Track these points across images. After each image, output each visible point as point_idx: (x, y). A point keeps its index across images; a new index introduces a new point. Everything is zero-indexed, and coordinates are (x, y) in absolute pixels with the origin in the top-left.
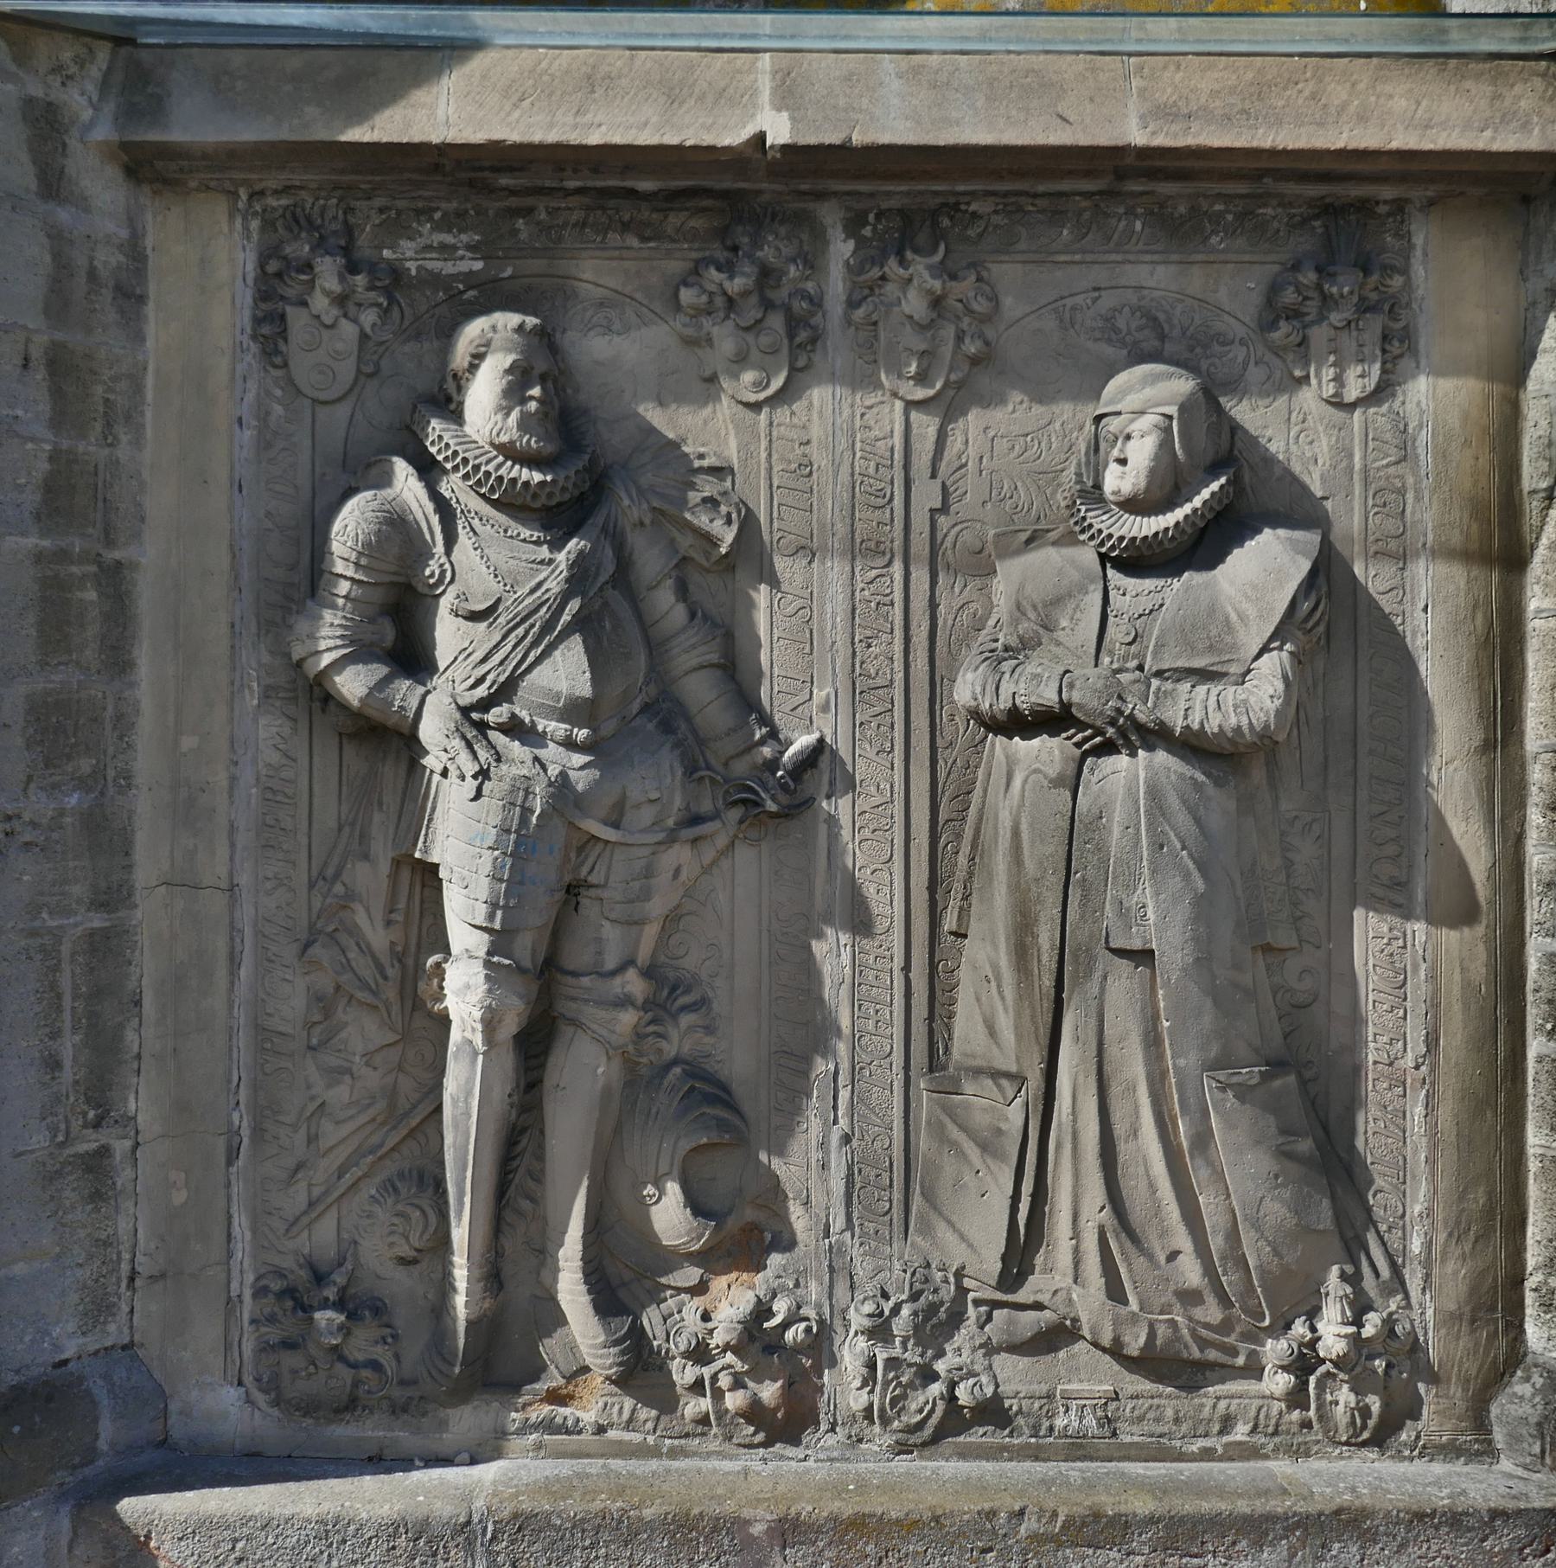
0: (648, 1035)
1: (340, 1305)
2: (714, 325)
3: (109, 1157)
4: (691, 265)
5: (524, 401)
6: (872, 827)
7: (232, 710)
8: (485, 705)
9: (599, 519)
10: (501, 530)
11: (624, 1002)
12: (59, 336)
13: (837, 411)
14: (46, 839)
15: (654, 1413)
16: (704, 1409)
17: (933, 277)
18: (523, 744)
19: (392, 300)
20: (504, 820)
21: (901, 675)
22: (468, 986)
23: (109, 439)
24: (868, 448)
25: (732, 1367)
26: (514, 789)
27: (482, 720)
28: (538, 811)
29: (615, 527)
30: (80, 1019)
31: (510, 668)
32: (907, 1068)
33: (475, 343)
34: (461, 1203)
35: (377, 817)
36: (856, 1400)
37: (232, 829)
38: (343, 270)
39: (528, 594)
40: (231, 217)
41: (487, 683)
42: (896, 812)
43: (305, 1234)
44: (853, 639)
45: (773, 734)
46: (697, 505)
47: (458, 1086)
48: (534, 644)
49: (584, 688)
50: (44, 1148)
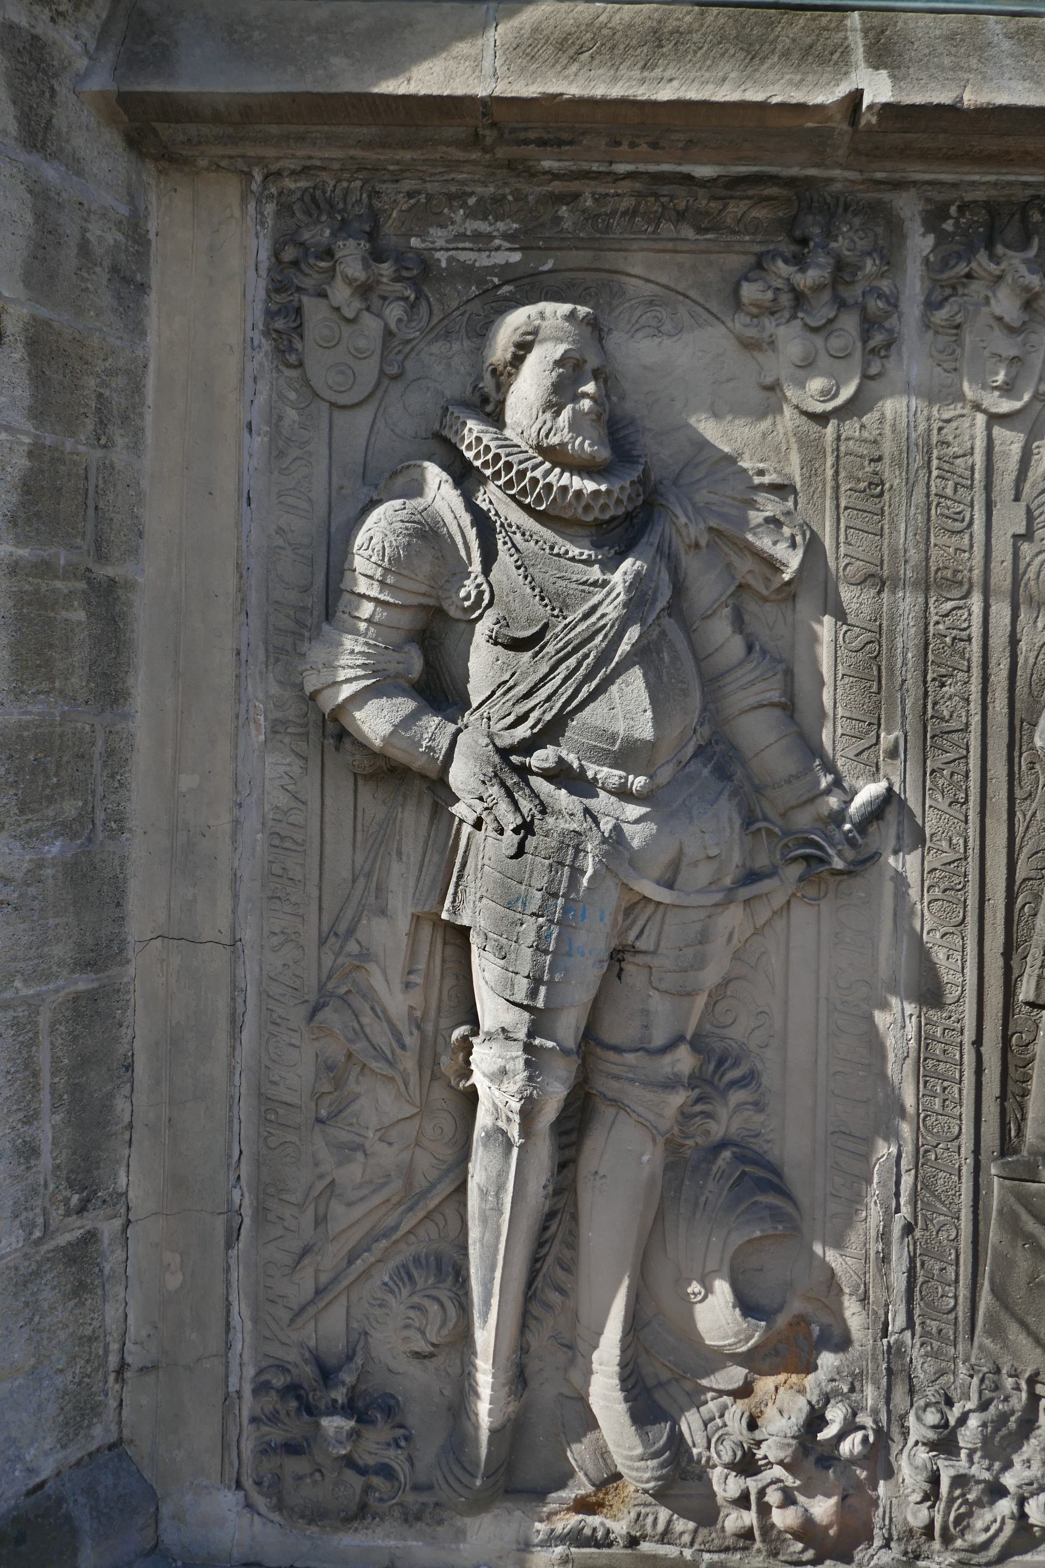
0: (695, 1115)
1: (348, 1409)
2: (778, 325)
3: (95, 1242)
4: (752, 259)
5: (576, 398)
6: (942, 887)
7: (236, 747)
8: (528, 747)
9: (653, 538)
10: (547, 547)
11: (670, 1084)
12: (44, 312)
13: (912, 424)
14: (20, 896)
15: (691, 1525)
16: (747, 1523)
17: (1032, 271)
18: (571, 792)
19: (420, 295)
20: (551, 882)
21: (978, 718)
22: (504, 1072)
23: (101, 439)
24: (946, 467)
25: (782, 1481)
26: (562, 846)
27: (523, 764)
28: (590, 872)
29: (670, 548)
30: (61, 1096)
31: (559, 705)
32: (977, 1151)
33: (520, 331)
34: (487, 1304)
35: (396, 868)
36: (915, 1515)
37: (235, 878)
38: (367, 255)
39: (581, 620)
40: (244, 199)
41: (531, 721)
42: (970, 870)
43: (312, 1323)
44: (925, 676)
45: (838, 783)
46: (759, 525)
47: (488, 1178)
48: (588, 678)
49: (645, 730)
50: (16, 1250)
